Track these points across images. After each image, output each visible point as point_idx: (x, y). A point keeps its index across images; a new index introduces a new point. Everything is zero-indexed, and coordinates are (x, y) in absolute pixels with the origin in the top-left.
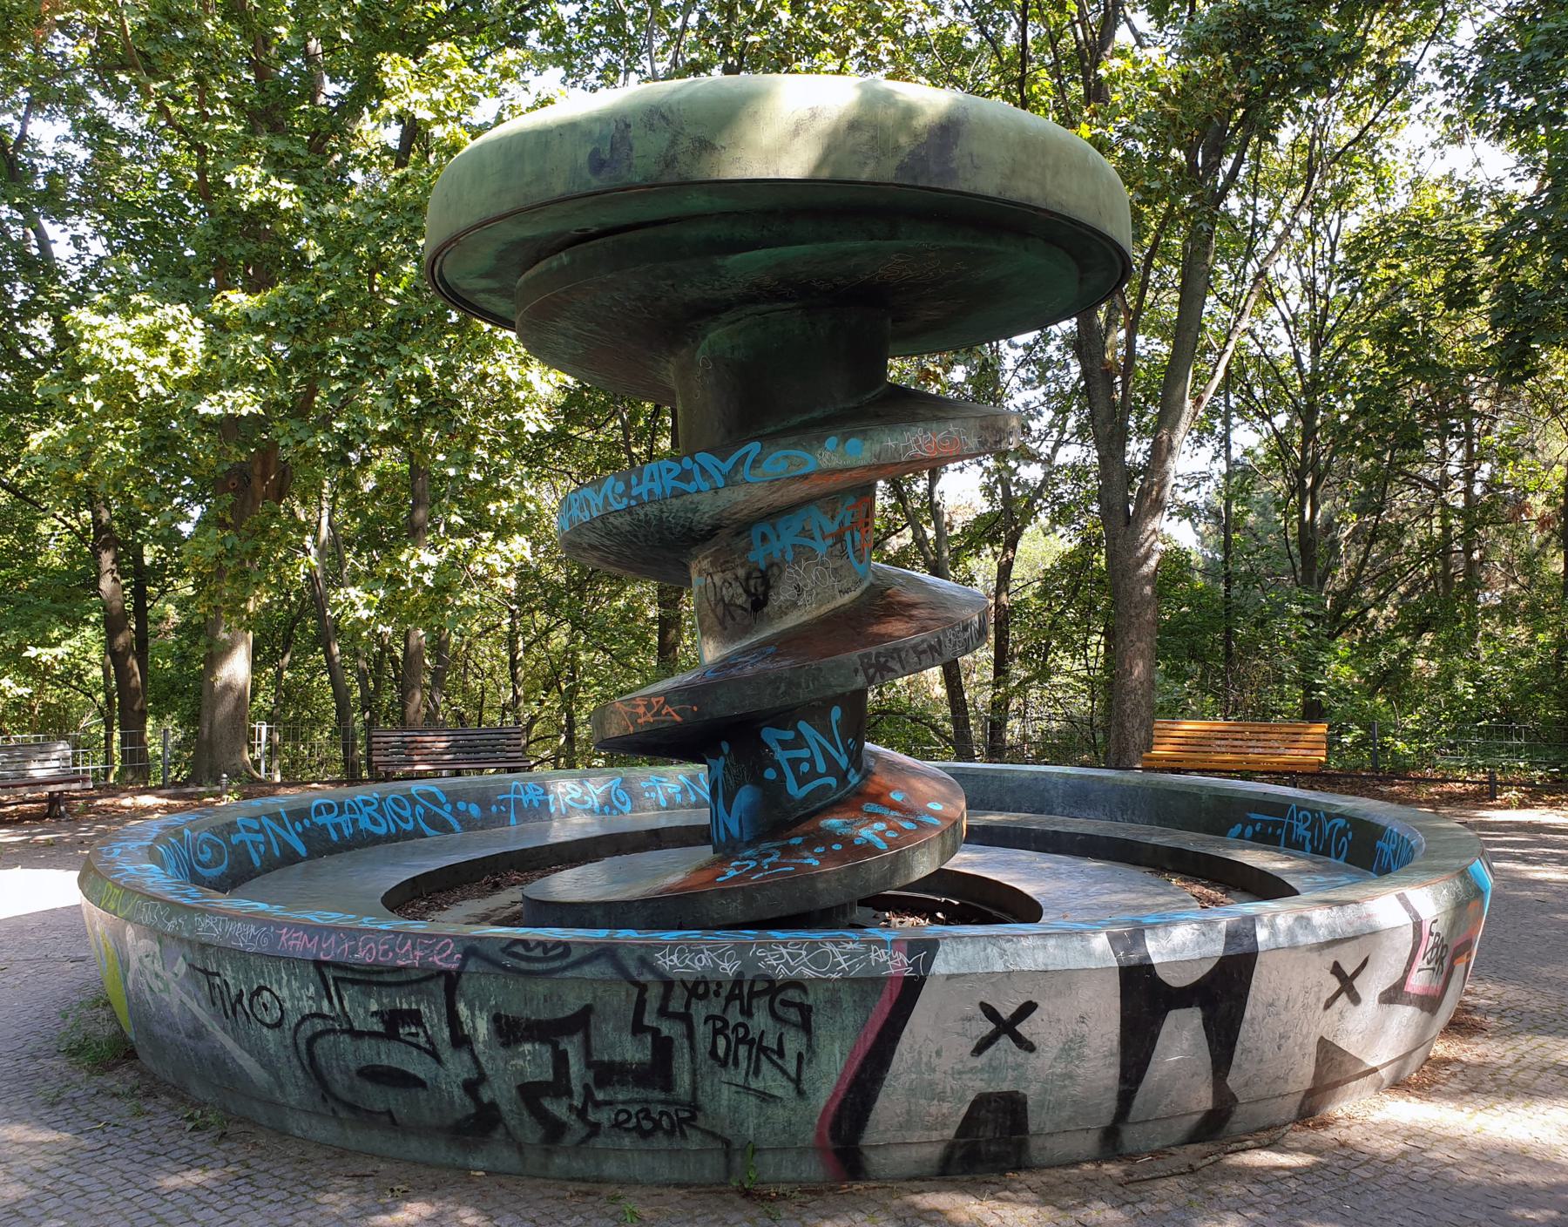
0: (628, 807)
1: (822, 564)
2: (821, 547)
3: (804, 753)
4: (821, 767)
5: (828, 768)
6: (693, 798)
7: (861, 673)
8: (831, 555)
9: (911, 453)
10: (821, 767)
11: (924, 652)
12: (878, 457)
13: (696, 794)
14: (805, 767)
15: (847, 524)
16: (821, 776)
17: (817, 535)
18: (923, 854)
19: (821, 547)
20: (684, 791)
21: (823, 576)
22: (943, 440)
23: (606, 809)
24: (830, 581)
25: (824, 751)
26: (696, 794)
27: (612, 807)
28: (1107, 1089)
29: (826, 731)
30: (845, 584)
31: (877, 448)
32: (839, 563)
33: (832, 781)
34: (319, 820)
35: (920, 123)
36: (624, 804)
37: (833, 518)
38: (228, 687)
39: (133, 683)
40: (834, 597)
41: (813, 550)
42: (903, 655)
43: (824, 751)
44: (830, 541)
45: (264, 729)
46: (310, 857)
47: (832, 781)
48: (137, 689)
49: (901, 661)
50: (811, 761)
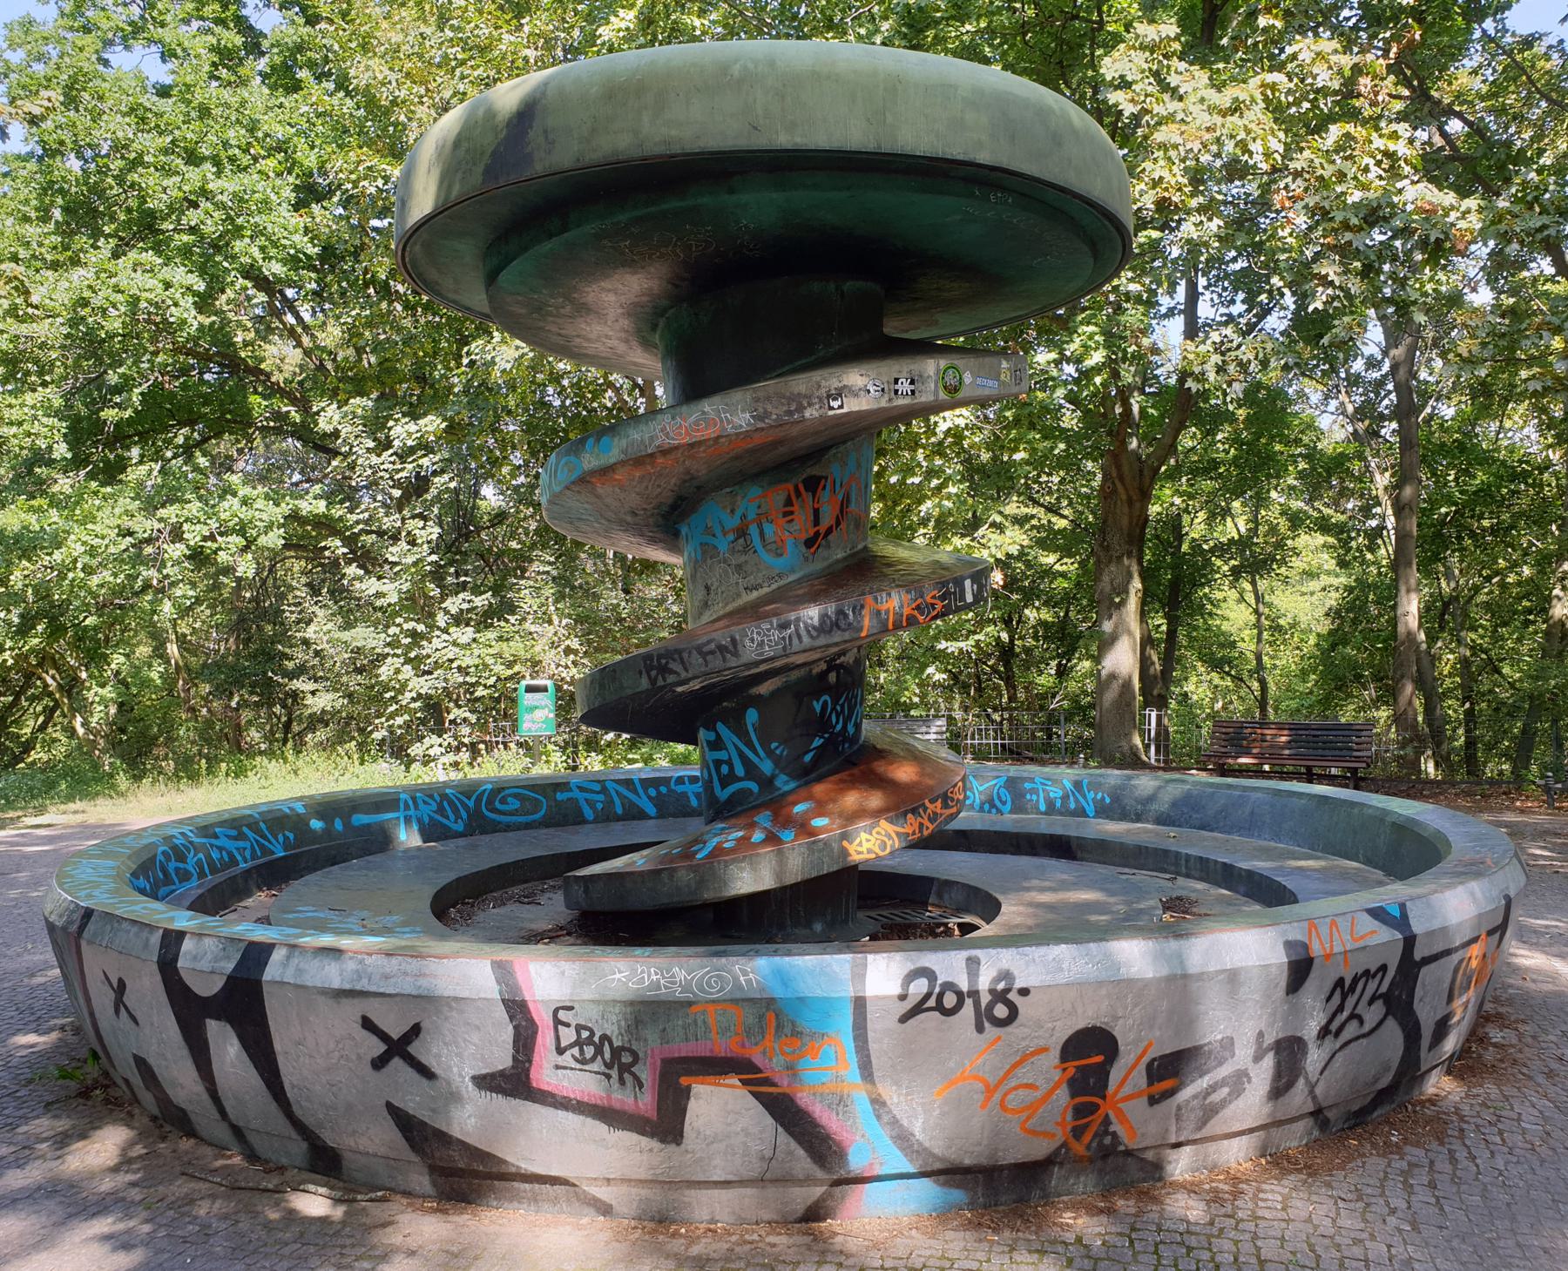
0: (1008, 807)
1: (725, 561)
2: (723, 545)
3: (723, 755)
4: (740, 770)
5: (747, 772)
6: (1073, 806)
7: (644, 675)
8: (733, 551)
9: (657, 443)
10: (740, 770)
11: (712, 652)
12: (625, 452)
13: (1076, 800)
14: (725, 769)
15: (751, 516)
16: (740, 779)
17: (718, 531)
18: (742, 870)
19: (723, 545)
20: (1065, 798)
21: (726, 572)
22: (696, 423)
23: (987, 807)
24: (734, 578)
25: (742, 755)
26: (1076, 800)
27: (993, 805)
28: (448, 1124)
29: (741, 732)
30: (751, 580)
31: (624, 442)
32: (743, 558)
33: (753, 786)
34: (680, 789)
35: (500, 118)
36: (1004, 803)
37: (732, 511)
38: (1113, 676)
39: (1152, 671)
40: (739, 595)
41: (715, 547)
42: (685, 655)
43: (742, 755)
44: (731, 537)
45: (1154, 715)
46: (595, 821)
47: (753, 786)
48: (1155, 677)
49: (683, 662)
50: (730, 763)
